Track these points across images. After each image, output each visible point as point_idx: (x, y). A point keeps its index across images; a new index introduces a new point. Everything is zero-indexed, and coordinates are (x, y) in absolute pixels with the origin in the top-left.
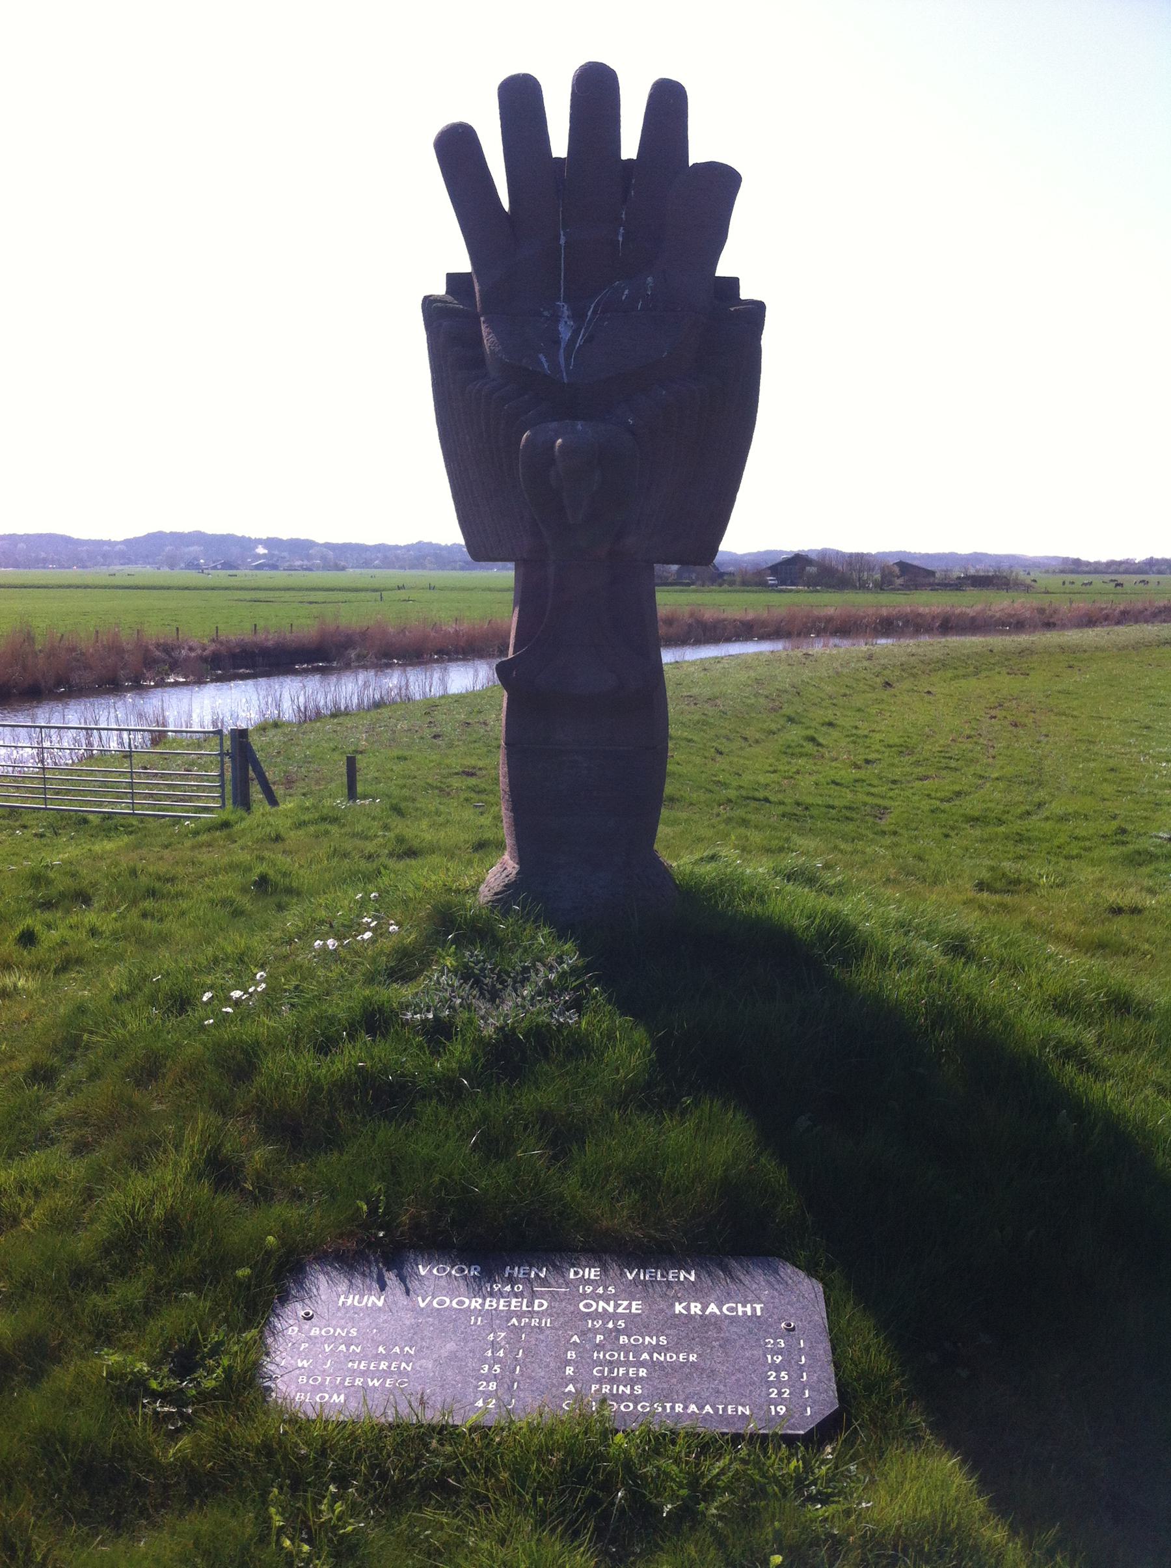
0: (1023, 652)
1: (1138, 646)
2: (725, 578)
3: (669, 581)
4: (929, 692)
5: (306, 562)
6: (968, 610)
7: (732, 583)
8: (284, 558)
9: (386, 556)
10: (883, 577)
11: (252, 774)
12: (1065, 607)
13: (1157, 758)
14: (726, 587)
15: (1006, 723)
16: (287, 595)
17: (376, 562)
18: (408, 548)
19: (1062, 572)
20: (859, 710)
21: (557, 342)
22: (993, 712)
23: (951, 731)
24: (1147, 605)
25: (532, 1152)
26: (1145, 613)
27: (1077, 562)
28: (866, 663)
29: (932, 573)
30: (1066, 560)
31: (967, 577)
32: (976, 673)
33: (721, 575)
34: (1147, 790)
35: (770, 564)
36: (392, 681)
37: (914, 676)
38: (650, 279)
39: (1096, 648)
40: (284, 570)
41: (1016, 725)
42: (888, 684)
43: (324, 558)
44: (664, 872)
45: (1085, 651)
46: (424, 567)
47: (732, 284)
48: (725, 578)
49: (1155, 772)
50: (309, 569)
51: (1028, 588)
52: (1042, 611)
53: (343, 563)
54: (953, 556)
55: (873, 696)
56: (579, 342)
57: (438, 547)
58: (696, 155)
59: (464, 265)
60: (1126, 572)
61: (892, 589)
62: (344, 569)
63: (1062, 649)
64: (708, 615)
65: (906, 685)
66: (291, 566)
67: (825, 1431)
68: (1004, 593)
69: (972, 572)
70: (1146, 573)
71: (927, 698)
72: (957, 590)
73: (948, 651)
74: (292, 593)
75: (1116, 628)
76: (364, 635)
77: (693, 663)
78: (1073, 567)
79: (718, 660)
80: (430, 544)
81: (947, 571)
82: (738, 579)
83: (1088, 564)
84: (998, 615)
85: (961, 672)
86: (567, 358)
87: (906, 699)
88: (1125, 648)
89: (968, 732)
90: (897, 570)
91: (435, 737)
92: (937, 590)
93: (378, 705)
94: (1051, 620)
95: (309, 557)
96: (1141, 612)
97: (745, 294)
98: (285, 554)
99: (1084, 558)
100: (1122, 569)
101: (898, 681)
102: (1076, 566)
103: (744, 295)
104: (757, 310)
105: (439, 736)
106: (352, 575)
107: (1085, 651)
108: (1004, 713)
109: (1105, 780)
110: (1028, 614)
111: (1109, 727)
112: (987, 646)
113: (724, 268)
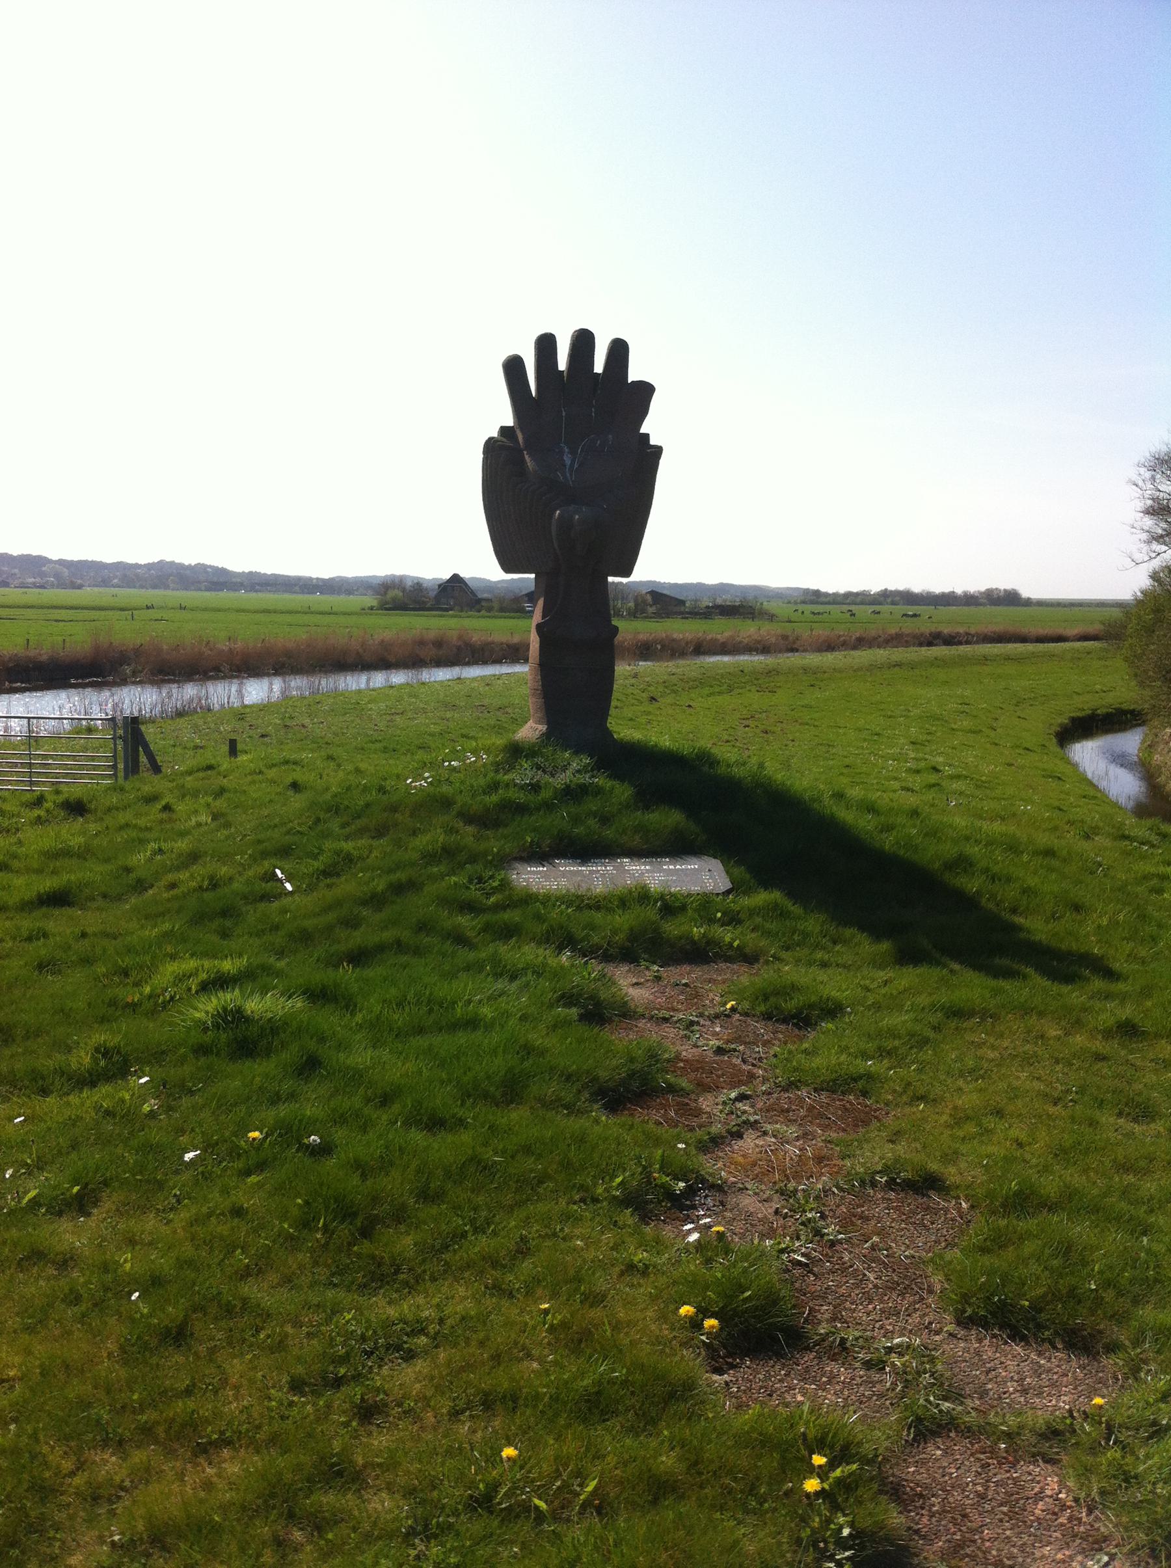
0: (770, 672)
1: (872, 668)
2: (483, 604)
3: (428, 605)
4: (690, 706)
5: (38, 580)
6: (719, 637)
7: (490, 609)
8: (15, 574)
9: (126, 574)
10: (636, 605)
11: (143, 759)
12: (806, 635)
13: (885, 758)
14: (483, 612)
15: (758, 731)
16: (30, 613)
17: (116, 581)
18: (149, 566)
19: (804, 602)
20: (631, 720)
21: (565, 466)
22: (746, 722)
23: (711, 737)
24: (881, 632)
25: (592, 822)
26: (879, 639)
27: (817, 593)
28: (633, 681)
29: (682, 602)
30: (807, 591)
31: (716, 607)
32: (730, 690)
33: (479, 601)
34: (875, 781)
35: (524, 592)
36: (190, 691)
37: (675, 692)
38: (610, 436)
39: (834, 669)
40: (15, 587)
41: (766, 732)
42: (653, 699)
43: (57, 575)
44: (609, 734)
45: (825, 672)
46: (167, 587)
47: (647, 436)
48: (483, 604)
49: (883, 768)
50: (42, 587)
51: (772, 617)
52: (785, 637)
53: (79, 581)
54: (700, 586)
55: (641, 708)
56: (576, 466)
57: (181, 566)
58: (632, 377)
59: (509, 421)
60: (862, 603)
61: (646, 617)
62: (80, 587)
63: (805, 670)
64: (476, 638)
65: (669, 699)
66: (23, 583)
67: (728, 892)
68: (749, 622)
69: (719, 601)
70: (880, 604)
71: (689, 711)
72: (706, 618)
73: (703, 670)
74: (33, 611)
75: (852, 652)
76: (138, 651)
77: (474, 679)
78: (812, 598)
79: (499, 677)
80: (172, 563)
81: (696, 601)
82: (496, 605)
83: (826, 595)
84: (746, 641)
85: (717, 689)
86: (571, 475)
87: (670, 712)
88: (860, 669)
89: (726, 737)
90: (649, 598)
91: (263, 736)
92: (687, 618)
93: (180, 714)
94: (795, 646)
95: (42, 575)
96: (875, 639)
97: (653, 442)
98: (16, 571)
99: (823, 590)
100: (859, 600)
101: (661, 696)
102: (815, 597)
103: (652, 443)
104: (658, 451)
105: (266, 736)
106: (89, 594)
107: (825, 672)
108: (756, 723)
109: (842, 774)
110: (773, 640)
111: (845, 734)
112: (738, 667)
113: (643, 430)
